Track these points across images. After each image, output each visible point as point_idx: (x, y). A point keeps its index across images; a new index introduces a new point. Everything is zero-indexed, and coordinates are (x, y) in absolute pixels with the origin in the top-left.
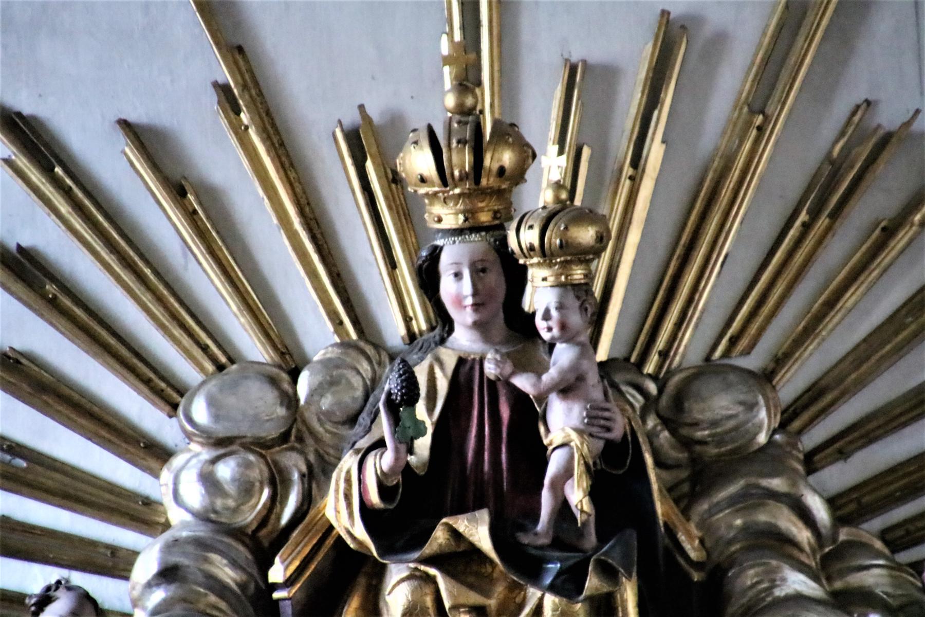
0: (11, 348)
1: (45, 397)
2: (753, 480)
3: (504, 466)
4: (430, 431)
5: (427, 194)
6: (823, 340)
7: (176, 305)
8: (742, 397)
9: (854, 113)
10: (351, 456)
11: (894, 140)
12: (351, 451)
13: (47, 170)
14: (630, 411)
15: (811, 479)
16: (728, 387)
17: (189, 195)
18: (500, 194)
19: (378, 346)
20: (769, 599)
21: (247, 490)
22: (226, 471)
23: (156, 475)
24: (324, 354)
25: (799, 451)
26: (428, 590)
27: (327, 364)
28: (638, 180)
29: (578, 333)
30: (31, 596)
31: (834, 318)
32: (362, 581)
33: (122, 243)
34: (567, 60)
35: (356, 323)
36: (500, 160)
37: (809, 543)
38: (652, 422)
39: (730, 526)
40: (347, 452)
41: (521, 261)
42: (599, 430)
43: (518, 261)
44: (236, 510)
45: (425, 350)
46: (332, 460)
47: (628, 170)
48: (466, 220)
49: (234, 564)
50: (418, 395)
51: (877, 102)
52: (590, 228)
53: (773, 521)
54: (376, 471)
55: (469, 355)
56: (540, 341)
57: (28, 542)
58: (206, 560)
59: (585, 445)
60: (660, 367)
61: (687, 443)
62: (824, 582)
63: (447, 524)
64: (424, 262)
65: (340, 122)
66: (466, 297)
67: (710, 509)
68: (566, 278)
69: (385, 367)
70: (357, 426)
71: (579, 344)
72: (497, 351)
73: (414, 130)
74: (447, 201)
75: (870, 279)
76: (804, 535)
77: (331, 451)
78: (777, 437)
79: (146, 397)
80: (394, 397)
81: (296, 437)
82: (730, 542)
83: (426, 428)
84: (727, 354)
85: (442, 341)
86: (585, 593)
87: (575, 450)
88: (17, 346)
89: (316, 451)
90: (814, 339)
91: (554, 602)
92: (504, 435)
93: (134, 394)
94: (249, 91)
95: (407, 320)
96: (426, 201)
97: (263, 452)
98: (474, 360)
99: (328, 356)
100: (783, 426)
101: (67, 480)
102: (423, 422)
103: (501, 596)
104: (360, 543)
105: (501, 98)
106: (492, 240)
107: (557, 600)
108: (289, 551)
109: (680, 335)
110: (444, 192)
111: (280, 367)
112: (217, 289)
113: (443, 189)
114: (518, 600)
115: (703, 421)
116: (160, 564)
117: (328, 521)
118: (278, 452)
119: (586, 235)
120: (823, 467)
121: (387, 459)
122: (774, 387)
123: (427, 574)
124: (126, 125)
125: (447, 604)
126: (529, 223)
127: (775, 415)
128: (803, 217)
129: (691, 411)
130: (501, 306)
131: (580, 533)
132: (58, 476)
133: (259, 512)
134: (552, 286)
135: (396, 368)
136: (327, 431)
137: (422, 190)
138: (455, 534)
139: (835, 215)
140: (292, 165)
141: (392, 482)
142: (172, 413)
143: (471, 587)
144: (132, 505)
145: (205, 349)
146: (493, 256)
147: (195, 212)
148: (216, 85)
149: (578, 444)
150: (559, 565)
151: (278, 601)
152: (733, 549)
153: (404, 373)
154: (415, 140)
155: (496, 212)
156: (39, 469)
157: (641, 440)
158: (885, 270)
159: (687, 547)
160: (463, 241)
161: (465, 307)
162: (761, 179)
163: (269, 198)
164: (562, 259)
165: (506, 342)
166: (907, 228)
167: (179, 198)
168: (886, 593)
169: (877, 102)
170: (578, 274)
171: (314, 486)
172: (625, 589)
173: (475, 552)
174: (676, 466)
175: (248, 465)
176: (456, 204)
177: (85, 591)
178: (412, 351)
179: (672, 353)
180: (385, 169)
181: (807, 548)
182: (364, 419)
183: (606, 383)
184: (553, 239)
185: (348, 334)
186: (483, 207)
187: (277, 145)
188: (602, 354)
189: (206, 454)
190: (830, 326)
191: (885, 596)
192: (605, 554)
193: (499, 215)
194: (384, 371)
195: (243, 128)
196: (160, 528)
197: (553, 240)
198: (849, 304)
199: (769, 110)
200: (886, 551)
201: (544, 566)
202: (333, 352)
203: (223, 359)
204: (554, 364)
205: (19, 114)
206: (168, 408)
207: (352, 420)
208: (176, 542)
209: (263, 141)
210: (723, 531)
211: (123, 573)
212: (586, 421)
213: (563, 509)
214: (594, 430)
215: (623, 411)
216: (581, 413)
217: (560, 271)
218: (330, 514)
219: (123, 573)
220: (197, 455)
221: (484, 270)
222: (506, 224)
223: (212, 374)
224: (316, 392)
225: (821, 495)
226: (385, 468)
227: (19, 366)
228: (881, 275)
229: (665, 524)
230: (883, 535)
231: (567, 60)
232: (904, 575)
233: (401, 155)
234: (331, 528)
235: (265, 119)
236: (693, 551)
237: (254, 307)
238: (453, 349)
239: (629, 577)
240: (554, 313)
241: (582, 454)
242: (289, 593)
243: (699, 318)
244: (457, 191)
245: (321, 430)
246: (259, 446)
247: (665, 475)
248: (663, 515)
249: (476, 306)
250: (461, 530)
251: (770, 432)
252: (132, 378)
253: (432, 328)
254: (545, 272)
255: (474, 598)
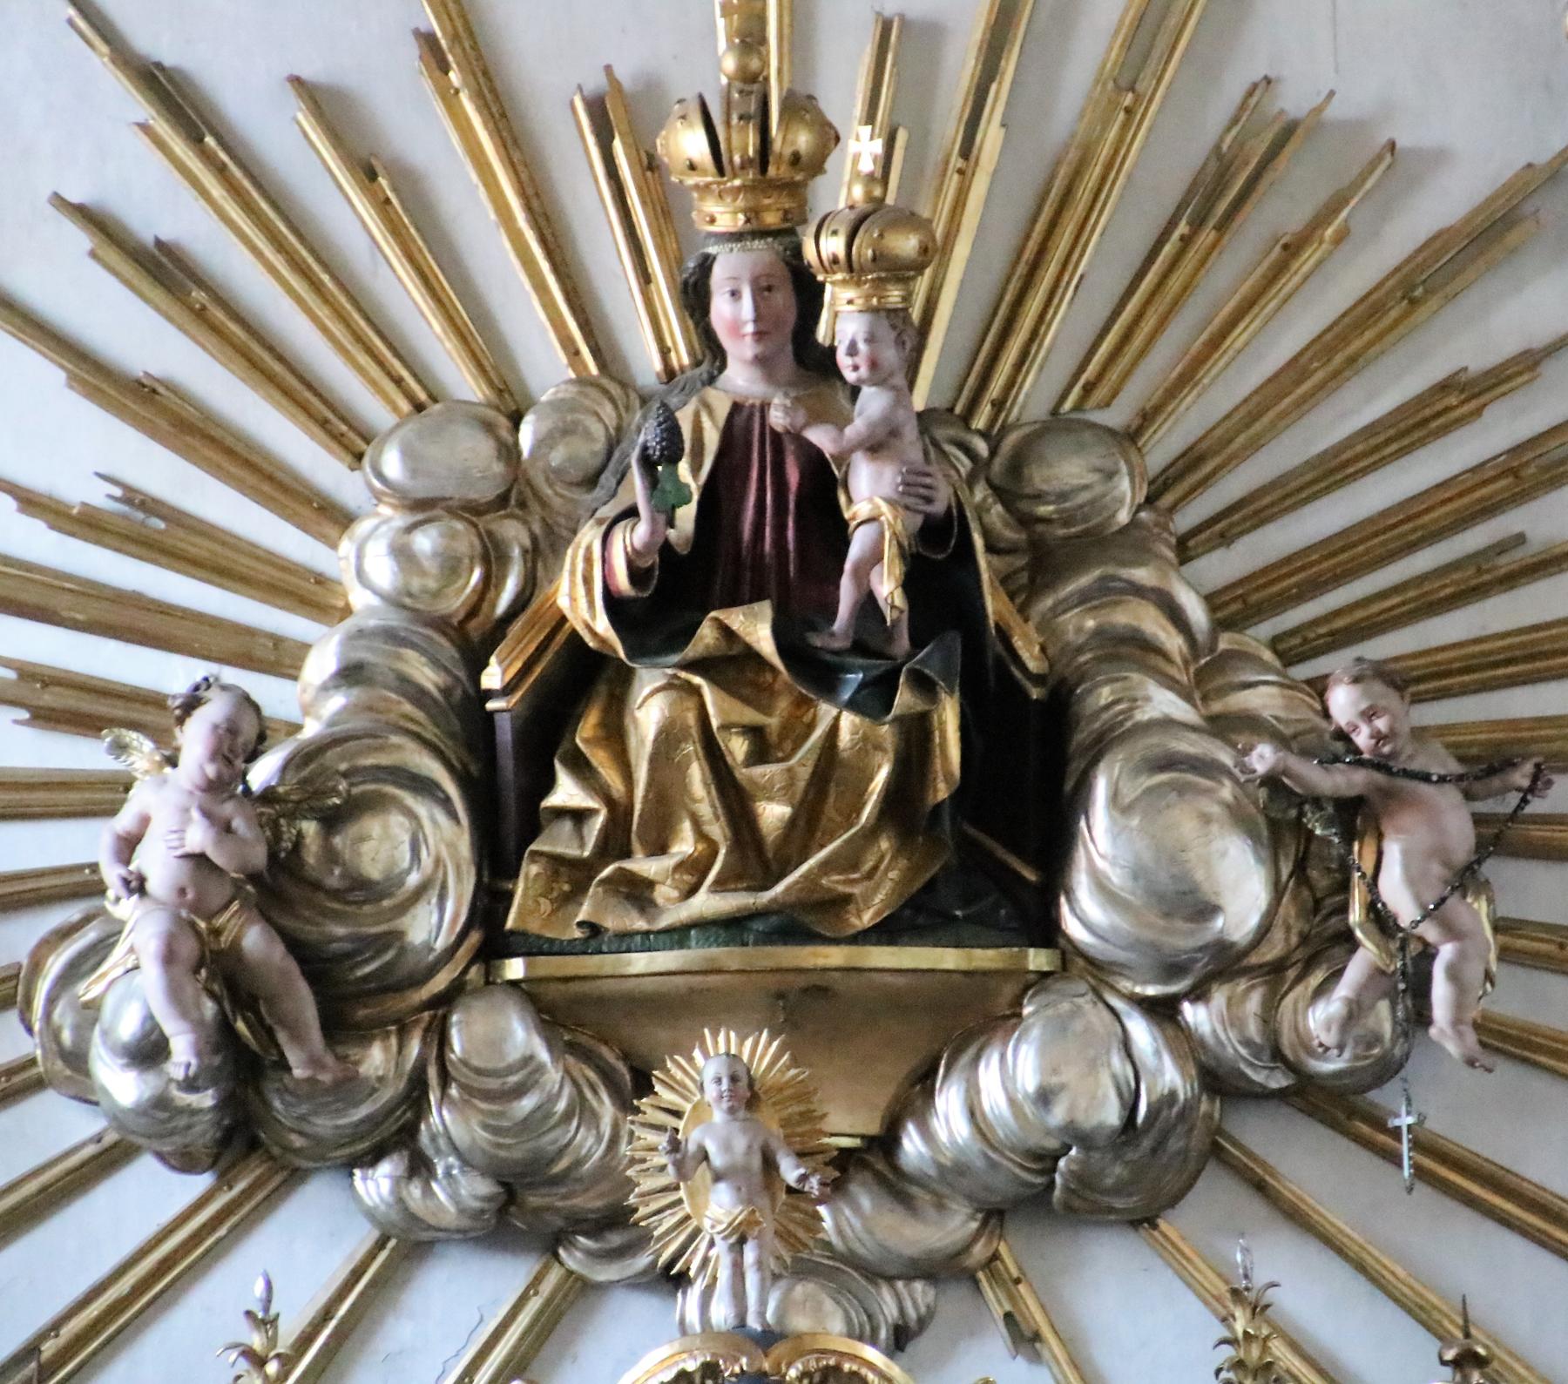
0: (146, 373)
1: (188, 439)
2: (1111, 570)
3: (791, 546)
4: (696, 497)
5: (697, 187)
6: (1205, 389)
7: (362, 323)
8: (1098, 462)
9: (1250, 94)
10: (592, 527)
11: (1300, 131)
12: (591, 522)
13: (196, 140)
14: (956, 477)
15: (1187, 569)
16: (1081, 448)
17: (380, 179)
18: (794, 189)
19: (625, 384)
20: (1129, 724)
21: (452, 568)
22: (425, 542)
23: (334, 546)
24: (557, 392)
25: (1171, 534)
26: (691, 703)
27: (557, 405)
28: (969, 172)
29: (891, 375)
30: (174, 697)
31: (1220, 361)
32: (602, 689)
33: (292, 238)
34: (878, 14)
35: (596, 352)
36: (793, 143)
37: (1181, 652)
38: (981, 492)
39: (1079, 630)
40: (586, 522)
41: (820, 278)
42: (920, 501)
43: (815, 277)
44: (436, 595)
45: (688, 391)
46: (565, 533)
47: (956, 161)
48: (748, 221)
49: (436, 663)
50: (682, 450)
51: (1279, 80)
52: (911, 236)
53: (1135, 623)
54: (625, 547)
55: (747, 398)
56: (839, 384)
57: (181, 630)
58: (399, 657)
59: (899, 521)
60: (992, 421)
61: (1026, 521)
62: (1199, 703)
63: (716, 619)
64: (691, 275)
65: (580, 88)
66: (745, 323)
67: (1055, 606)
68: (879, 301)
69: (634, 413)
70: (598, 489)
71: (894, 388)
72: (786, 395)
73: (680, 101)
74: (725, 196)
75: (1266, 311)
76: (1173, 642)
77: (562, 521)
78: (1143, 515)
79: (320, 443)
80: (651, 452)
81: (517, 501)
82: (1080, 650)
83: (691, 494)
84: (1078, 407)
85: (711, 380)
86: (895, 711)
87: (886, 527)
88: (152, 371)
89: (543, 520)
90: (1192, 388)
91: (853, 722)
92: (792, 506)
93: (305, 438)
94: (460, 43)
95: (664, 352)
96: (695, 195)
97: (474, 519)
98: (753, 406)
99: (560, 395)
100: (1150, 501)
101: (217, 548)
102: (687, 486)
103: (785, 714)
104: (603, 641)
105: (792, 62)
106: (781, 248)
107: (857, 720)
108: (506, 651)
109: (1020, 379)
110: (719, 183)
111: (498, 409)
112: (416, 304)
113: (719, 179)
114: (807, 719)
115: (1048, 493)
116: (339, 660)
117: (560, 611)
118: (494, 520)
119: (906, 244)
120: (1198, 556)
121: (640, 533)
122: (1139, 450)
123: (689, 683)
124: (297, 82)
125: (715, 723)
126: (833, 228)
127: (1141, 488)
128: (1183, 228)
129: (1031, 479)
130: (790, 336)
131: (889, 634)
132: (206, 543)
133: (468, 597)
134: (860, 311)
135: (653, 414)
136: (557, 494)
137: (691, 180)
138: (727, 633)
139: (1222, 227)
140: (515, 141)
141: (645, 563)
142: (355, 465)
143: (747, 701)
144: (302, 583)
145: (398, 381)
146: (783, 272)
147: (387, 201)
148: (417, 34)
149: (890, 517)
150: (861, 676)
151: (492, 714)
152: (1082, 659)
153: (665, 421)
154: (681, 114)
155: (786, 212)
156: (181, 533)
157: (968, 514)
158: (1285, 301)
159: (1025, 655)
160: (743, 249)
161: (744, 336)
162: (1129, 176)
163: (486, 185)
164: (875, 275)
165: (792, 384)
166: (1315, 245)
167: (367, 181)
168: (1276, 718)
169: (1279, 80)
170: (894, 295)
171: (540, 565)
172: (944, 709)
173: (752, 656)
174: (1011, 551)
175: (453, 535)
176: (735, 200)
177: (244, 692)
178: (672, 391)
179: (1008, 404)
180: (637, 150)
181: (1178, 660)
182: (608, 479)
183: (927, 441)
184: (864, 250)
185: (585, 367)
186: (770, 205)
187: (497, 116)
188: (919, 401)
189: (400, 520)
190: (1214, 372)
191: (1274, 722)
192: (921, 661)
193: (790, 216)
194: (633, 418)
195: (452, 91)
196: (338, 614)
197: (864, 250)
198: (1239, 344)
199: (1140, 87)
200: (1277, 664)
201: (841, 676)
202: (566, 390)
203: (422, 396)
204: (860, 414)
205: (159, 65)
206: (349, 458)
207: (591, 481)
208: (361, 633)
209: (479, 109)
210: (1071, 636)
211: (291, 671)
212: (901, 489)
213: (868, 604)
214: (911, 501)
215: (947, 476)
216: (894, 479)
217: (871, 291)
218: (563, 602)
219: (291, 671)
220: (387, 521)
221: (769, 289)
222: (799, 229)
223: (408, 415)
224: (544, 443)
225: (1197, 593)
226: (638, 543)
227: (157, 397)
228: (1278, 309)
229: (997, 626)
230: (1274, 643)
231: (878, 14)
232: (1300, 695)
233: (664, 133)
234: (563, 619)
235: (481, 80)
236: (1032, 659)
237: (463, 329)
238: (725, 391)
239: (951, 693)
240: (862, 347)
241: (895, 533)
242: (508, 702)
243: (1046, 358)
244: (737, 182)
245: (549, 492)
246: (471, 511)
247: (995, 560)
248: (994, 613)
249: (759, 335)
250: (735, 627)
251: (1134, 509)
252: (303, 417)
253: (697, 363)
254: (850, 293)
255: (751, 716)
